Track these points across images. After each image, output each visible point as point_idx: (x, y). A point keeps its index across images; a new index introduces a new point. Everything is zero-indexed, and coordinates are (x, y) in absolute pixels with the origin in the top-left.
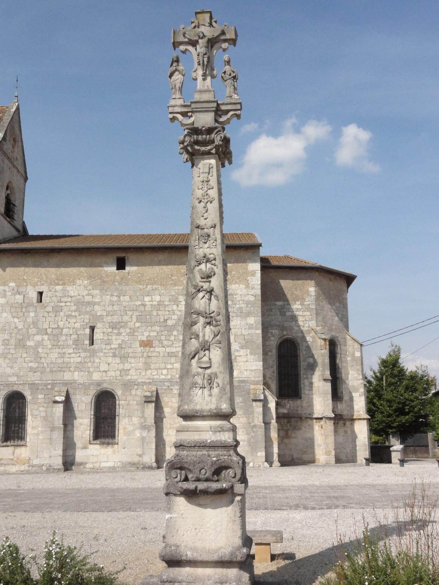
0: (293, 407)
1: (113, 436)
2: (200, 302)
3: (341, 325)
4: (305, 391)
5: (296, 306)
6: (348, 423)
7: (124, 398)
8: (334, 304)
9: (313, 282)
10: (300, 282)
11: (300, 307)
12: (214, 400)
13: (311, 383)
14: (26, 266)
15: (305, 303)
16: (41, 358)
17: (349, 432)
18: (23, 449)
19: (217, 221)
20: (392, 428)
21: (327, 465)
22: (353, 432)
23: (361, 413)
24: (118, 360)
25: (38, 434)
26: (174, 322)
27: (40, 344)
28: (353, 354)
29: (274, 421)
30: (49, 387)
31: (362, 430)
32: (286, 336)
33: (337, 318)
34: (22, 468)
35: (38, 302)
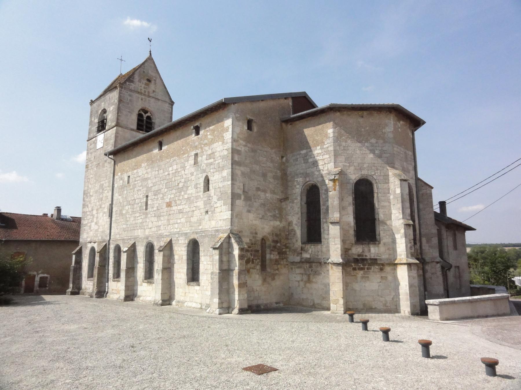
0: (315, 252)
5: (317, 151)
6: (388, 269)
10: (320, 127)
11: (320, 152)
15: (325, 146)
17: (390, 278)
28: (395, 191)
32: (308, 183)
33: (371, 156)
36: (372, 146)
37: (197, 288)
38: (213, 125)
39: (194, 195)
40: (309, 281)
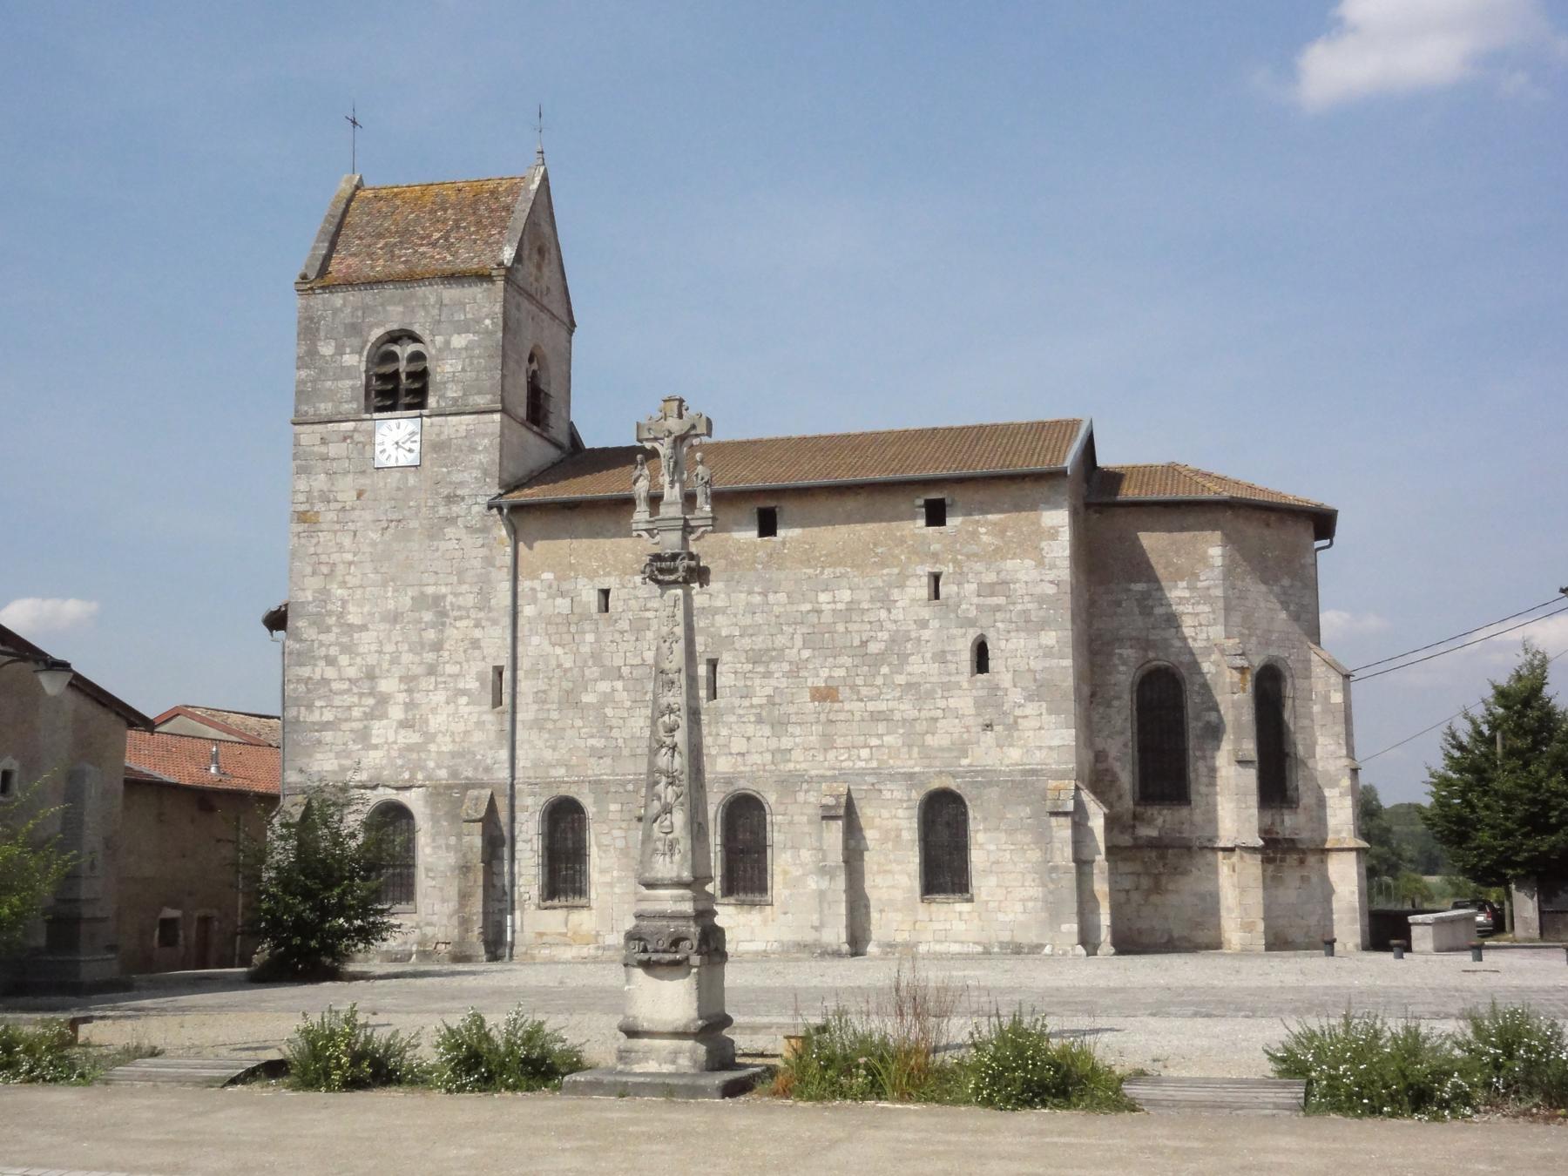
1: (763, 889)
2: (663, 760)
3: (1296, 630)
4: (1198, 788)
5: (1177, 593)
6: (1312, 860)
7: (781, 809)
8: (1277, 580)
9: (1218, 534)
10: (1186, 535)
12: (675, 867)
13: (1213, 771)
14: (574, 535)
15: (1199, 585)
16: (611, 728)
17: (1315, 879)
18: (585, 913)
19: (682, 664)
20: (1514, 865)
21: (1246, 952)
22: (1325, 879)
23: (1344, 834)
24: (767, 731)
25: (611, 885)
26: (882, 646)
27: (607, 699)
28: (1327, 697)
29: (1101, 858)
30: (630, 787)
31: (1345, 878)
33: (1283, 615)
34: (585, 951)
35: (600, 611)
36: (1285, 593)
37: (966, 907)
38: (1001, 511)
39: (933, 679)
40: (1157, 888)
